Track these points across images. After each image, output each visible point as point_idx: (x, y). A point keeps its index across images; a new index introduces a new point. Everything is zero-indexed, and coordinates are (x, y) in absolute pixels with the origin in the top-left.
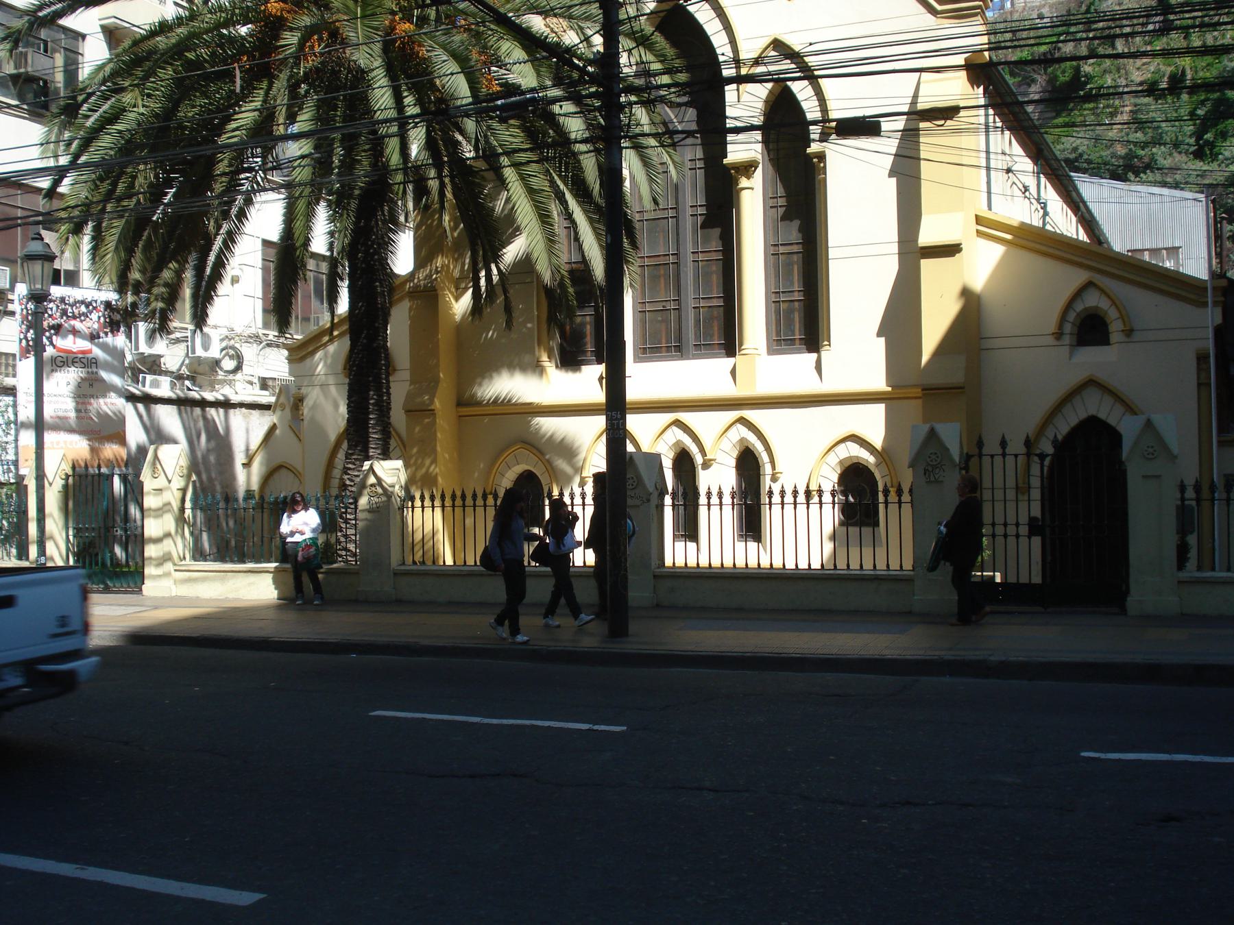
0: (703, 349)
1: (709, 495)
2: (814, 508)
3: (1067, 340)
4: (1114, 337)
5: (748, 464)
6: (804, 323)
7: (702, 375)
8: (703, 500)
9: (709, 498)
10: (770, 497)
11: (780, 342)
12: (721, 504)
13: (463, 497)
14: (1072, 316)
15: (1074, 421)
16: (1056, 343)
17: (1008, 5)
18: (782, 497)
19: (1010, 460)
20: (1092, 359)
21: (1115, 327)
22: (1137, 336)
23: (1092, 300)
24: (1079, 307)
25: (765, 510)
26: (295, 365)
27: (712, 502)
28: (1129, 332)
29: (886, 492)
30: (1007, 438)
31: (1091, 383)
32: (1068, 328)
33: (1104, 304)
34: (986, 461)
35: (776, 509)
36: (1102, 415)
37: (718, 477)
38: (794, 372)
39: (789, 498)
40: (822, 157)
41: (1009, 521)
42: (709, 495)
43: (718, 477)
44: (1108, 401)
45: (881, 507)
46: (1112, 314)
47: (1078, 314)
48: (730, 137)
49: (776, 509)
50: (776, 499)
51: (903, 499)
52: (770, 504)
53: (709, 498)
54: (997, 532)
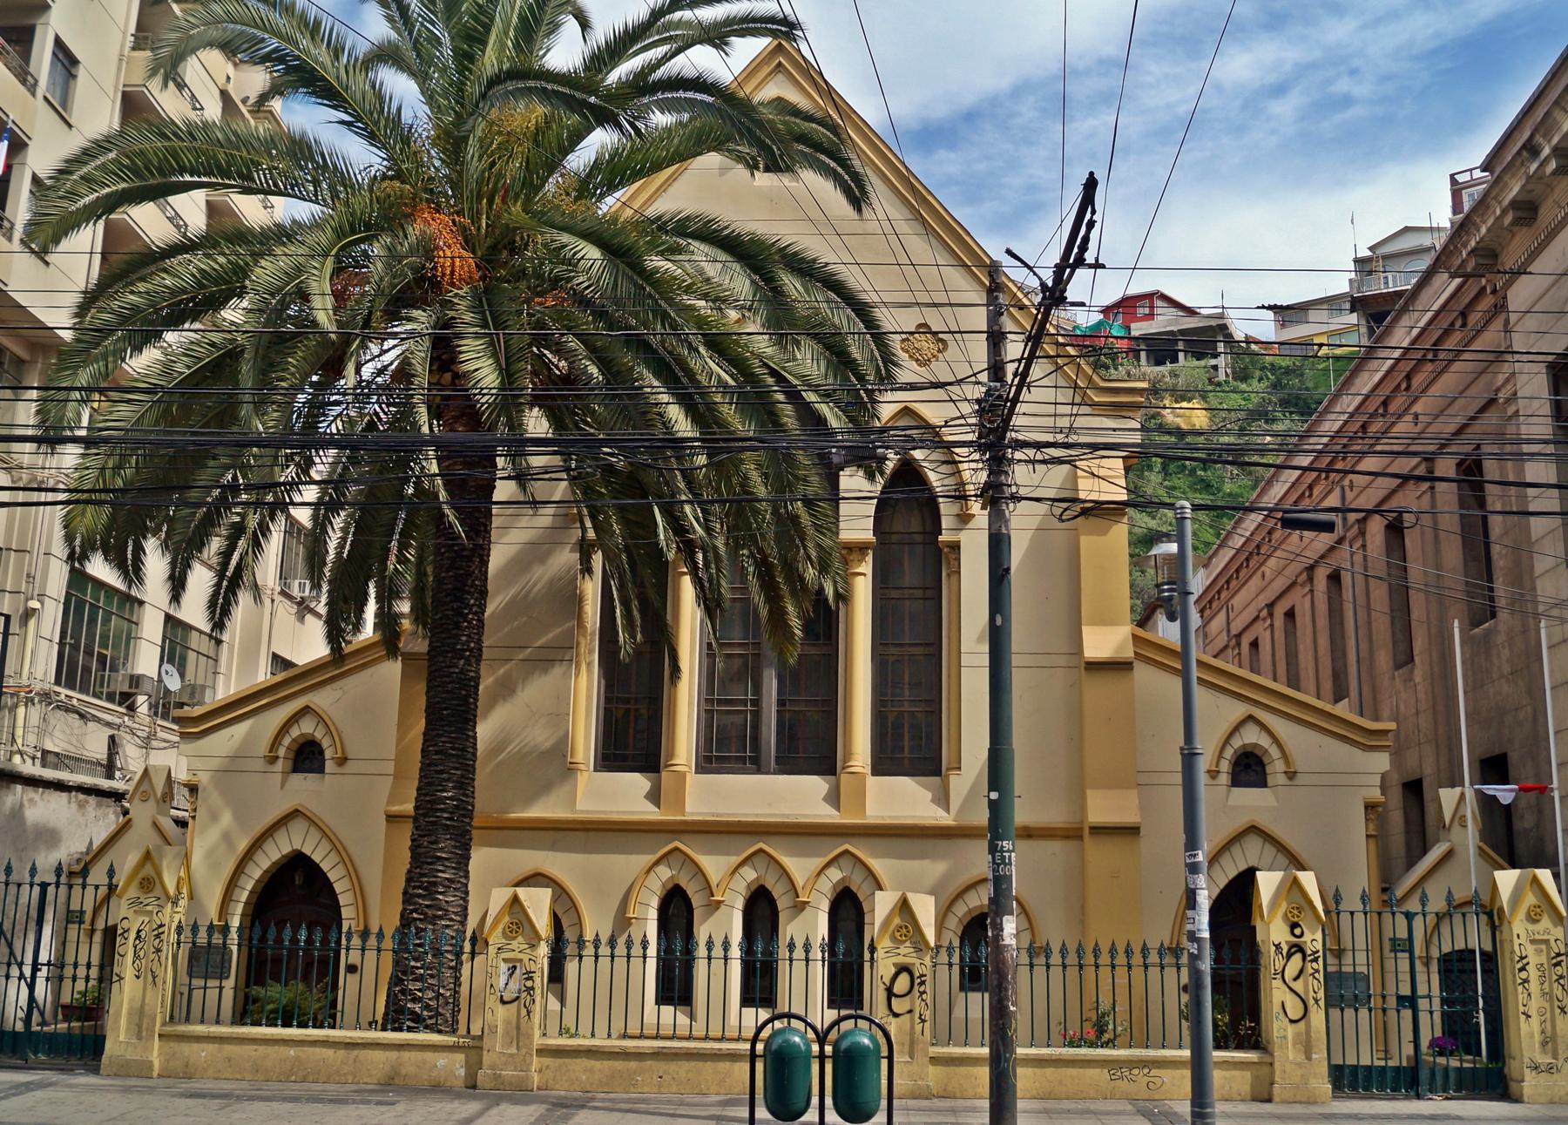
0: (789, 763)
1: (710, 945)
2: (1040, 971)
3: (1224, 778)
4: (329, 766)
6: (912, 744)
7: (800, 796)
8: (702, 951)
9: (709, 949)
13: (1080, 952)
14: (287, 741)
15: (275, 856)
19: (90, 891)
20: (303, 790)
21: (1276, 768)
22: (1300, 779)
23: (1251, 736)
25: (783, 968)
27: (633, 952)
28: (1291, 775)
29: (349, 934)
31: (295, 814)
32: (282, 752)
33: (1264, 741)
34: (1345, 918)
35: (799, 966)
36: (307, 851)
38: (901, 799)
40: (955, 547)
44: (314, 836)
46: (1274, 752)
47: (294, 740)
51: (601, 952)
53: (709, 949)
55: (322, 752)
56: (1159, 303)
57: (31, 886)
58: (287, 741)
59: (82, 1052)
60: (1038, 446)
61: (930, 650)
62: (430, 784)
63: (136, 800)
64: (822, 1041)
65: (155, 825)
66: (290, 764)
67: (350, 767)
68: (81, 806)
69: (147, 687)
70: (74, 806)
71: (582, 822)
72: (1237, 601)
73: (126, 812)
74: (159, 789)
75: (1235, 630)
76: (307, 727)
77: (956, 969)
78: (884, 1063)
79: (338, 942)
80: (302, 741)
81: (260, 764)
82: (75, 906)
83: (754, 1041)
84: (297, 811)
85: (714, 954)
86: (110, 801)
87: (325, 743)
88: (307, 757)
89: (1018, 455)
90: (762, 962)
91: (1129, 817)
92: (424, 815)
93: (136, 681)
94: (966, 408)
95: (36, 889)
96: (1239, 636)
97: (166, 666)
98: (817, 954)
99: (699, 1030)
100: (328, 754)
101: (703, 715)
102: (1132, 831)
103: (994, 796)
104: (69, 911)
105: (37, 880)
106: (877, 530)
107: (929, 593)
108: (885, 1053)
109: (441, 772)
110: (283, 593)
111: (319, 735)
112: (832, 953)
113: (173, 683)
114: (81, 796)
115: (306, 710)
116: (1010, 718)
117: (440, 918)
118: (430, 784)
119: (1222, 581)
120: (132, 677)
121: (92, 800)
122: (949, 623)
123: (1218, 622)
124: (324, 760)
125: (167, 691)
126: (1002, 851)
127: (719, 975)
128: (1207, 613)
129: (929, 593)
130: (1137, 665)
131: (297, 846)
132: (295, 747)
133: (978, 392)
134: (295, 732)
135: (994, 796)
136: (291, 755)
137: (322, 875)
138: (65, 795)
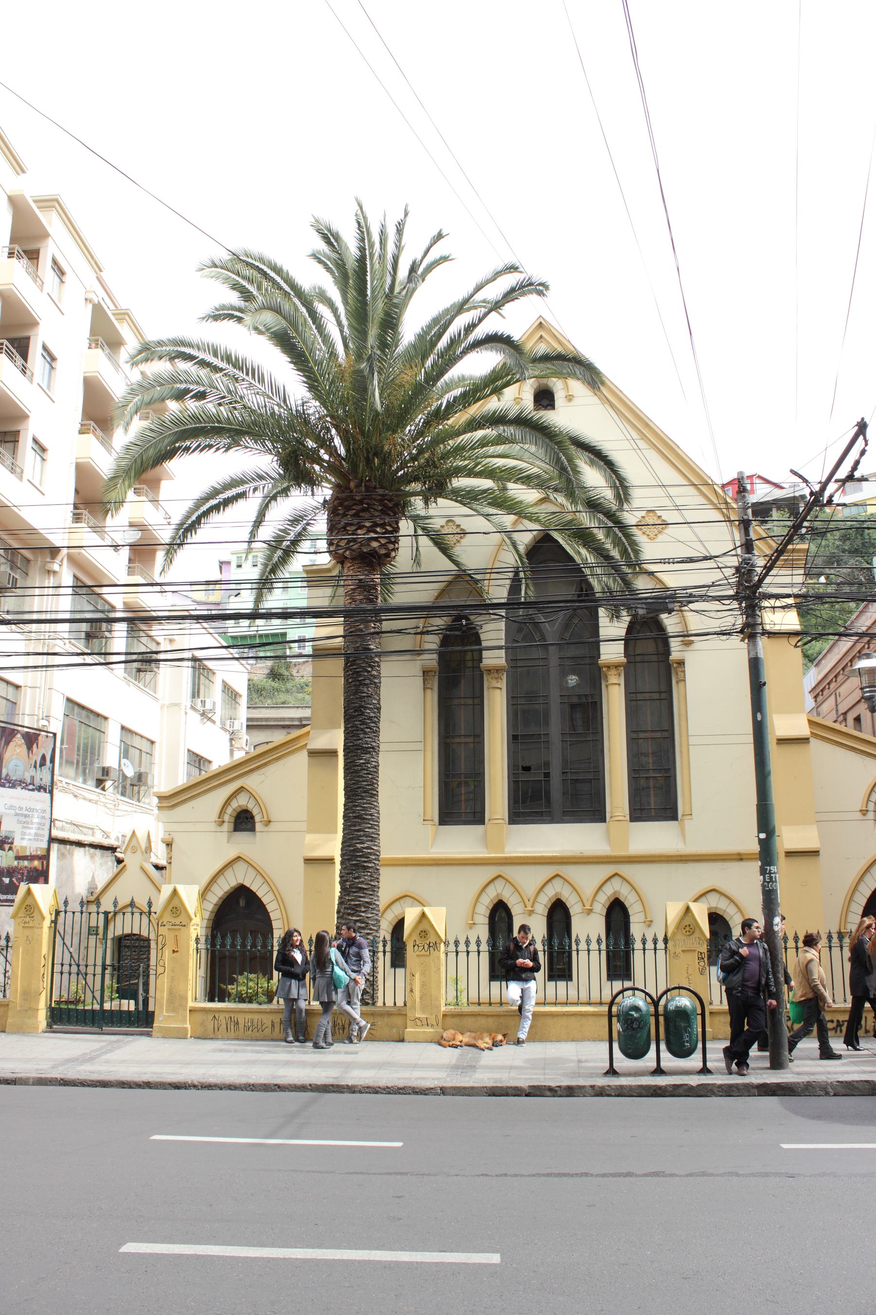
1: (644, 942)
3: (227, 827)
4: (258, 827)
5: (617, 915)
6: (657, 798)
8: (638, 945)
10: (786, 942)
11: (640, 812)
12: (655, 949)
14: (229, 810)
16: (862, 818)
17: (871, 550)
18: (644, 944)
20: (243, 844)
24: (235, 804)
26: (167, 813)
30: (69, 900)
32: (227, 818)
35: (583, 955)
37: (588, 927)
39: (650, 945)
40: (681, 663)
41: (64, 962)
42: (644, 942)
43: (588, 927)
44: (252, 873)
45: (574, 954)
48: (503, 643)
49: (583, 955)
50: (583, 946)
52: (578, 951)
54: (72, 971)
55: (252, 817)
56: (758, 481)
57: (98, 913)
58: (229, 810)
59: (138, 1022)
60: (777, 597)
61: (666, 734)
62: (352, 839)
63: (129, 852)
64: (656, 1003)
65: (142, 869)
66: (232, 825)
67: (272, 826)
68: (92, 857)
69: (113, 775)
70: (88, 857)
71: (434, 860)
72: (842, 690)
73: (119, 861)
74: (143, 844)
75: (842, 710)
76: (242, 801)
77: (604, 954)
78: (699, 1017)
79: (570, 946)
80: (239, 810)
81: (859, 815)
82: (93, 923)
83: (611, 1004)
84: (239, 857)
85: (647, 947)
86: (109, 853)
87: (255, 811)
88: (244, 821)
89: (765, 603)
90: (558, 952)
91: (811, 844)
92: (349, 860)
93: (106, 771)
94: (729, 572)
95: (102, 916)
96: (845, 714)
97: (124, 761)
98: (594, 946)
99: (584, 997)
100: (257, 818)
101: (512, 784)
102: (815, 853)
103: (763, 836)
104: (89, 927)
105: (102, 910)
106: (626, 654)
107: (664, 696)
108: (699, 1011)
109: (359, 830)
110: (193, 708)
111: (251, 806)
112: (213, 945)
113: (130, 772)
114: (92, 850)
115: (241, 789)
116: (770, 785)
117: (363, 928)
118: (352, 839)
119: (832, 676)
120: (103, 768)
121: (98, 852)
122: (679, 715)
123: (830, 703)
124: (254, 823)
125: (125, 777)
126: (770, 873)
127: (590, 963)
128: (820, 698)
129: (664, 696)
130: (812, 740)
131: (241, 881)
132: (235, 814)
133: (734, 562)
134: (235, 804)
135: (763, 836)
136: (233, 820)
137: (259, 900)
138: (82, 849)
